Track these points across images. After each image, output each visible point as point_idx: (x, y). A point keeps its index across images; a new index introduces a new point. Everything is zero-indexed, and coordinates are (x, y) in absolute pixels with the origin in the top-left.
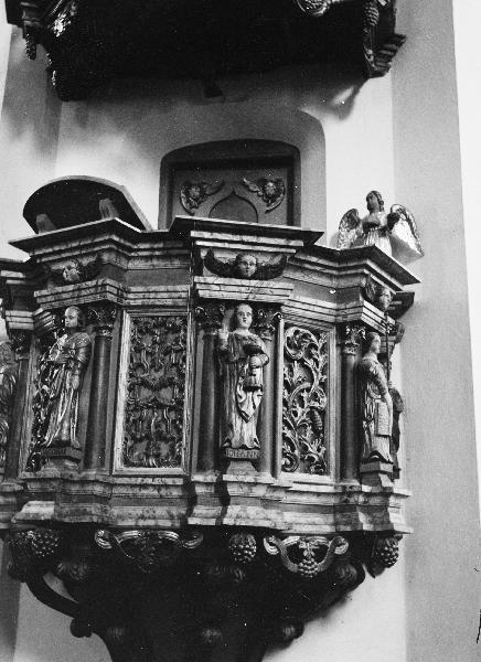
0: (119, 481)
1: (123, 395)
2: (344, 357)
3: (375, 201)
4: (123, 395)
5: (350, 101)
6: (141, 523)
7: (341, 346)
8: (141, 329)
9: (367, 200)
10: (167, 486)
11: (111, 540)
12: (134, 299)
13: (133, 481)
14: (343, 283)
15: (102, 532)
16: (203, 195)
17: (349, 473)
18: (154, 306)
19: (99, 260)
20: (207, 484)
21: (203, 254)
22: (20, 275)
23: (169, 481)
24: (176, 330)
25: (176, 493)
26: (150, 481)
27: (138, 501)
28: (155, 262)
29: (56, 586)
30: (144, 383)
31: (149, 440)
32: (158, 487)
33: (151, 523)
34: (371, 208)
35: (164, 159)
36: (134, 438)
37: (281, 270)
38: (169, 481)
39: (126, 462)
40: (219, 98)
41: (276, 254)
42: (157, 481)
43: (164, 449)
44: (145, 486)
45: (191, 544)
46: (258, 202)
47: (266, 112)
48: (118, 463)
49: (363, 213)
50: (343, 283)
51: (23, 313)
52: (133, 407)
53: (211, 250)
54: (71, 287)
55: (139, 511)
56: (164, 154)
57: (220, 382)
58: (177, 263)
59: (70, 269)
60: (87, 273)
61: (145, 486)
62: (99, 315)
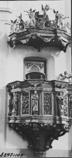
0: (44, 117)
1: (43, 104)
2: (69, 100)
3: (66, 73)
4: (43, 104)
5: (58, 54)
6: (48, 123)
7: (69, 98)
8: (45, 95)
9: (65, 72)
10: (51, 118)
11: (43, 125)
12: (44, 89)
13: (46, 117)
14: (69, 88)
15: (42, 124)
16: (30, 65)
17: (70, 116)
18: (47, 91)
19: (40, 84)
20: (52, 118)
21: (56, 85)
22: (20, 83)
23: (51, 117)
24: (50, 95)
25: (52, 119)
26: (48, 117)
27: (46, 120)
28: (47, 85)
29: (61, 133)
30: (46, 103)
31: (48, 111)
32: (49, 118)
33: (49, 123)
34: (65, 74)
35: (24, 59)
36: (45, 111)
37: (65, 87)
38: (51, 117)
39: (44, 114)
40: (37, 50)
41: (64, 85)
42: (50, 117)
43: (49, 112)
44: (48, 118)
45: (55, 126)
46: (40, 68)
47: (44, 53)
48: (43, 114)
49: (63, 74)
50: (69, 88)
51: (19, 89)
52: (44, 106)
53: (57, 84)
54: (35, 88)
55: (47, 121)
56: (26, 57)
57: (58, 103)
58: (50, 85)
59: (36, 85)
60: (38, 86)
61: (48, 118)
62: (39, 92)
